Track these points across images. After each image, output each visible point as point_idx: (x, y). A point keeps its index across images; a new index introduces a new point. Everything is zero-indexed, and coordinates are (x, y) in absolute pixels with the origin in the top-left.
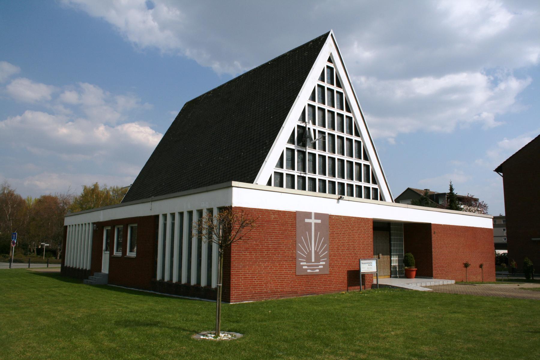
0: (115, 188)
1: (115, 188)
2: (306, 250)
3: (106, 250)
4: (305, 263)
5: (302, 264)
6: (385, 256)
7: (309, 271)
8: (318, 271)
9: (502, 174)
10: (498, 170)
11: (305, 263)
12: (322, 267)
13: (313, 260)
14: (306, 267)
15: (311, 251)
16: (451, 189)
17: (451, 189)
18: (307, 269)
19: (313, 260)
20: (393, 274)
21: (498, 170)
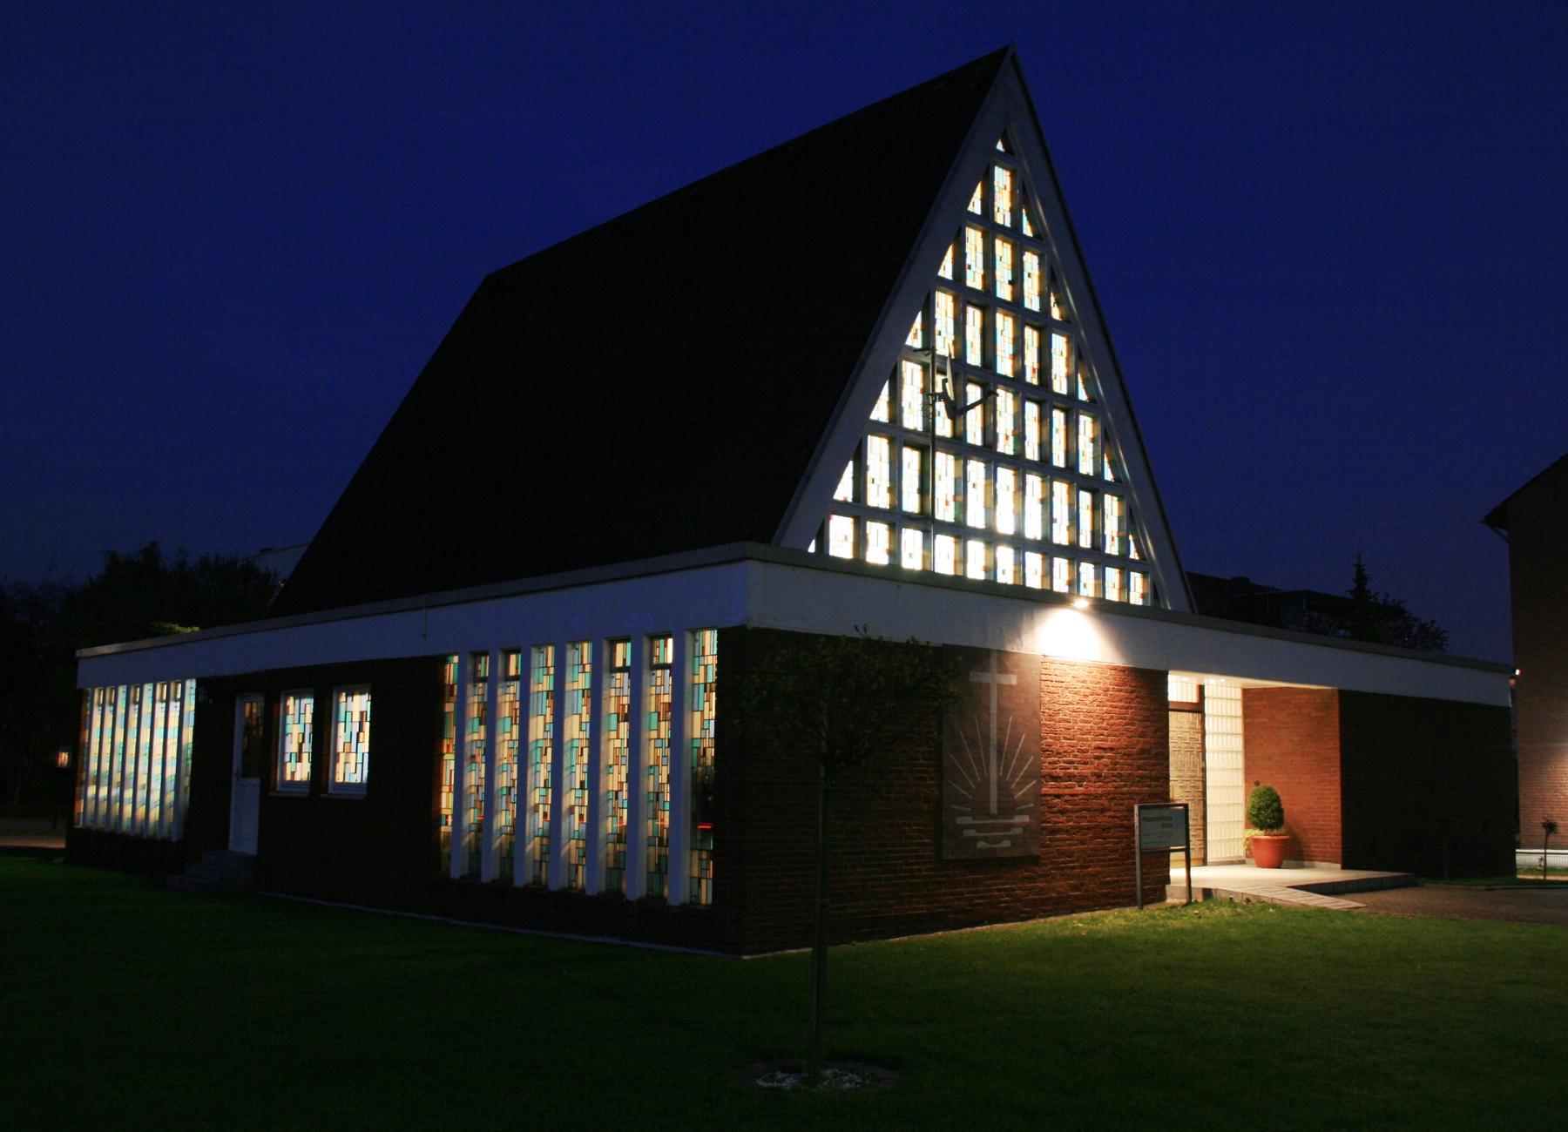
0: (212, 560)
1: (212, 560)
2: (973, 777)
3: (246, 773)
4: (969, 820)
5: (961, 820)
6: (357, 698)
7: (981, 845)
8: (1006, 843)
9: (1505, 533)
10: (1496, 519)
11: (969, 820)
12: (1018, 831)
13: (994, 810)
14: (972, 833)
15: (986, 781)
16: (1361, 578)
17: (1361, 578)
18: (974, 840)
19: (994, 810)
20: (248, 729)
21: (1496, 519)
